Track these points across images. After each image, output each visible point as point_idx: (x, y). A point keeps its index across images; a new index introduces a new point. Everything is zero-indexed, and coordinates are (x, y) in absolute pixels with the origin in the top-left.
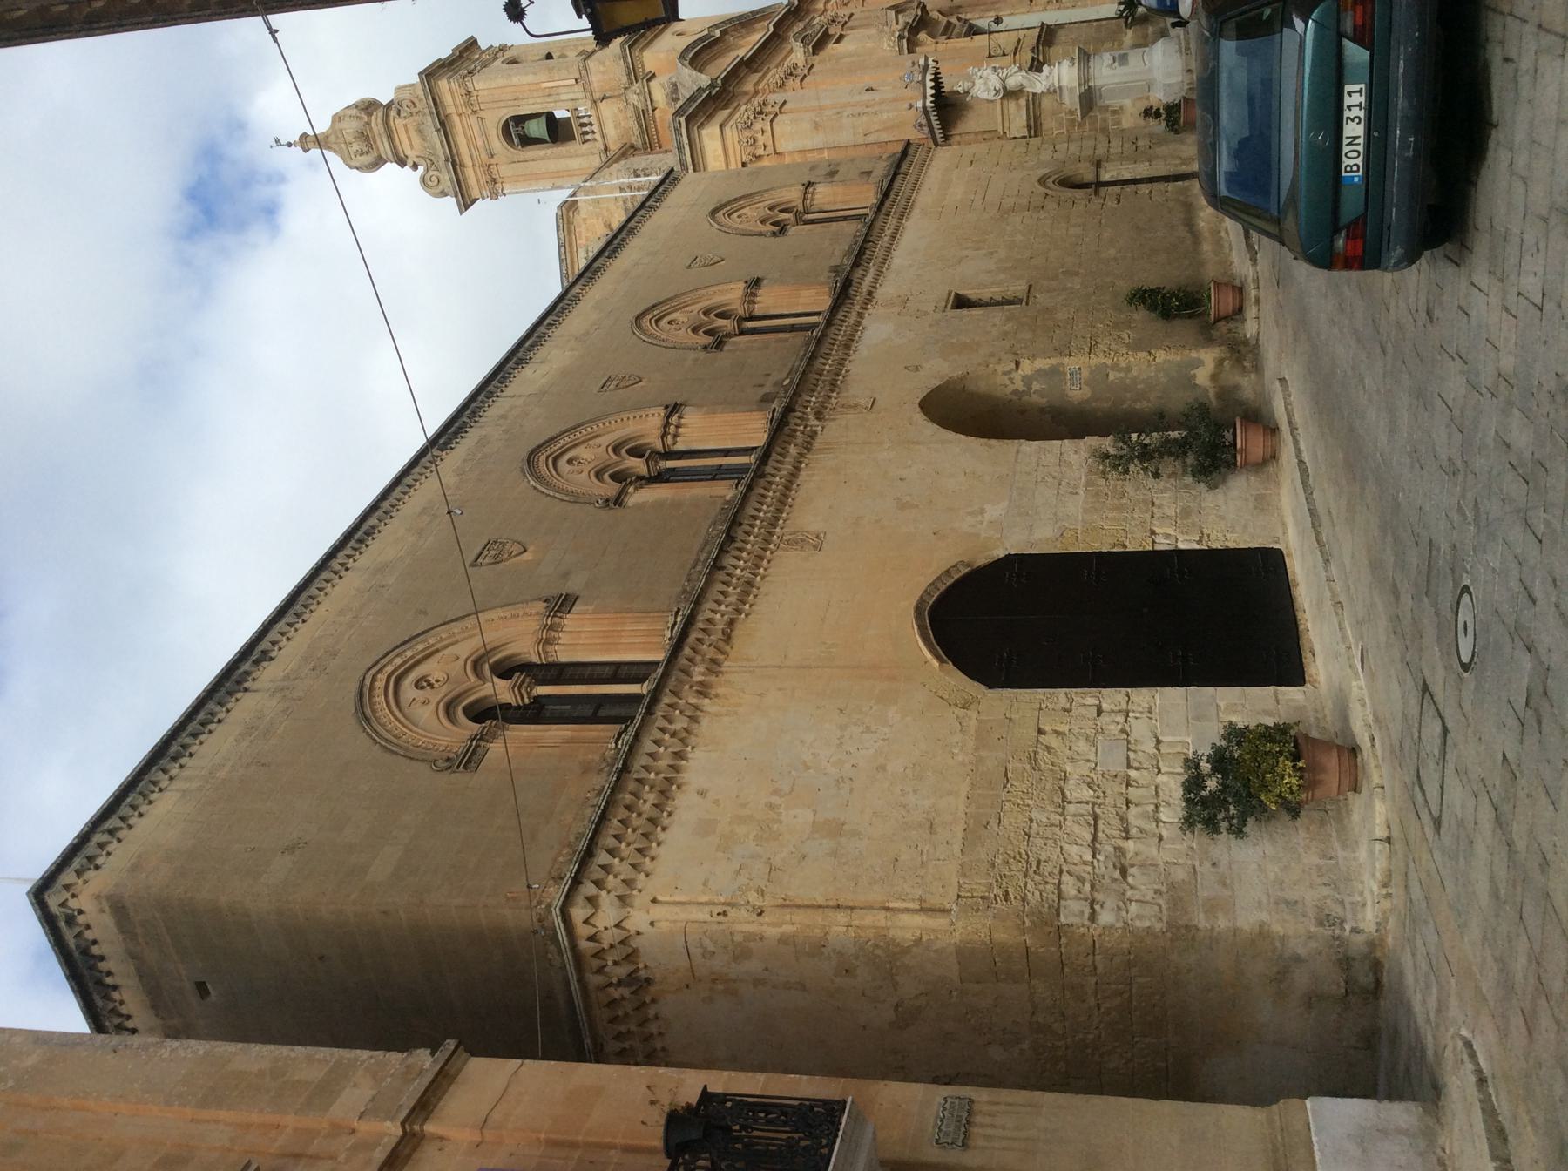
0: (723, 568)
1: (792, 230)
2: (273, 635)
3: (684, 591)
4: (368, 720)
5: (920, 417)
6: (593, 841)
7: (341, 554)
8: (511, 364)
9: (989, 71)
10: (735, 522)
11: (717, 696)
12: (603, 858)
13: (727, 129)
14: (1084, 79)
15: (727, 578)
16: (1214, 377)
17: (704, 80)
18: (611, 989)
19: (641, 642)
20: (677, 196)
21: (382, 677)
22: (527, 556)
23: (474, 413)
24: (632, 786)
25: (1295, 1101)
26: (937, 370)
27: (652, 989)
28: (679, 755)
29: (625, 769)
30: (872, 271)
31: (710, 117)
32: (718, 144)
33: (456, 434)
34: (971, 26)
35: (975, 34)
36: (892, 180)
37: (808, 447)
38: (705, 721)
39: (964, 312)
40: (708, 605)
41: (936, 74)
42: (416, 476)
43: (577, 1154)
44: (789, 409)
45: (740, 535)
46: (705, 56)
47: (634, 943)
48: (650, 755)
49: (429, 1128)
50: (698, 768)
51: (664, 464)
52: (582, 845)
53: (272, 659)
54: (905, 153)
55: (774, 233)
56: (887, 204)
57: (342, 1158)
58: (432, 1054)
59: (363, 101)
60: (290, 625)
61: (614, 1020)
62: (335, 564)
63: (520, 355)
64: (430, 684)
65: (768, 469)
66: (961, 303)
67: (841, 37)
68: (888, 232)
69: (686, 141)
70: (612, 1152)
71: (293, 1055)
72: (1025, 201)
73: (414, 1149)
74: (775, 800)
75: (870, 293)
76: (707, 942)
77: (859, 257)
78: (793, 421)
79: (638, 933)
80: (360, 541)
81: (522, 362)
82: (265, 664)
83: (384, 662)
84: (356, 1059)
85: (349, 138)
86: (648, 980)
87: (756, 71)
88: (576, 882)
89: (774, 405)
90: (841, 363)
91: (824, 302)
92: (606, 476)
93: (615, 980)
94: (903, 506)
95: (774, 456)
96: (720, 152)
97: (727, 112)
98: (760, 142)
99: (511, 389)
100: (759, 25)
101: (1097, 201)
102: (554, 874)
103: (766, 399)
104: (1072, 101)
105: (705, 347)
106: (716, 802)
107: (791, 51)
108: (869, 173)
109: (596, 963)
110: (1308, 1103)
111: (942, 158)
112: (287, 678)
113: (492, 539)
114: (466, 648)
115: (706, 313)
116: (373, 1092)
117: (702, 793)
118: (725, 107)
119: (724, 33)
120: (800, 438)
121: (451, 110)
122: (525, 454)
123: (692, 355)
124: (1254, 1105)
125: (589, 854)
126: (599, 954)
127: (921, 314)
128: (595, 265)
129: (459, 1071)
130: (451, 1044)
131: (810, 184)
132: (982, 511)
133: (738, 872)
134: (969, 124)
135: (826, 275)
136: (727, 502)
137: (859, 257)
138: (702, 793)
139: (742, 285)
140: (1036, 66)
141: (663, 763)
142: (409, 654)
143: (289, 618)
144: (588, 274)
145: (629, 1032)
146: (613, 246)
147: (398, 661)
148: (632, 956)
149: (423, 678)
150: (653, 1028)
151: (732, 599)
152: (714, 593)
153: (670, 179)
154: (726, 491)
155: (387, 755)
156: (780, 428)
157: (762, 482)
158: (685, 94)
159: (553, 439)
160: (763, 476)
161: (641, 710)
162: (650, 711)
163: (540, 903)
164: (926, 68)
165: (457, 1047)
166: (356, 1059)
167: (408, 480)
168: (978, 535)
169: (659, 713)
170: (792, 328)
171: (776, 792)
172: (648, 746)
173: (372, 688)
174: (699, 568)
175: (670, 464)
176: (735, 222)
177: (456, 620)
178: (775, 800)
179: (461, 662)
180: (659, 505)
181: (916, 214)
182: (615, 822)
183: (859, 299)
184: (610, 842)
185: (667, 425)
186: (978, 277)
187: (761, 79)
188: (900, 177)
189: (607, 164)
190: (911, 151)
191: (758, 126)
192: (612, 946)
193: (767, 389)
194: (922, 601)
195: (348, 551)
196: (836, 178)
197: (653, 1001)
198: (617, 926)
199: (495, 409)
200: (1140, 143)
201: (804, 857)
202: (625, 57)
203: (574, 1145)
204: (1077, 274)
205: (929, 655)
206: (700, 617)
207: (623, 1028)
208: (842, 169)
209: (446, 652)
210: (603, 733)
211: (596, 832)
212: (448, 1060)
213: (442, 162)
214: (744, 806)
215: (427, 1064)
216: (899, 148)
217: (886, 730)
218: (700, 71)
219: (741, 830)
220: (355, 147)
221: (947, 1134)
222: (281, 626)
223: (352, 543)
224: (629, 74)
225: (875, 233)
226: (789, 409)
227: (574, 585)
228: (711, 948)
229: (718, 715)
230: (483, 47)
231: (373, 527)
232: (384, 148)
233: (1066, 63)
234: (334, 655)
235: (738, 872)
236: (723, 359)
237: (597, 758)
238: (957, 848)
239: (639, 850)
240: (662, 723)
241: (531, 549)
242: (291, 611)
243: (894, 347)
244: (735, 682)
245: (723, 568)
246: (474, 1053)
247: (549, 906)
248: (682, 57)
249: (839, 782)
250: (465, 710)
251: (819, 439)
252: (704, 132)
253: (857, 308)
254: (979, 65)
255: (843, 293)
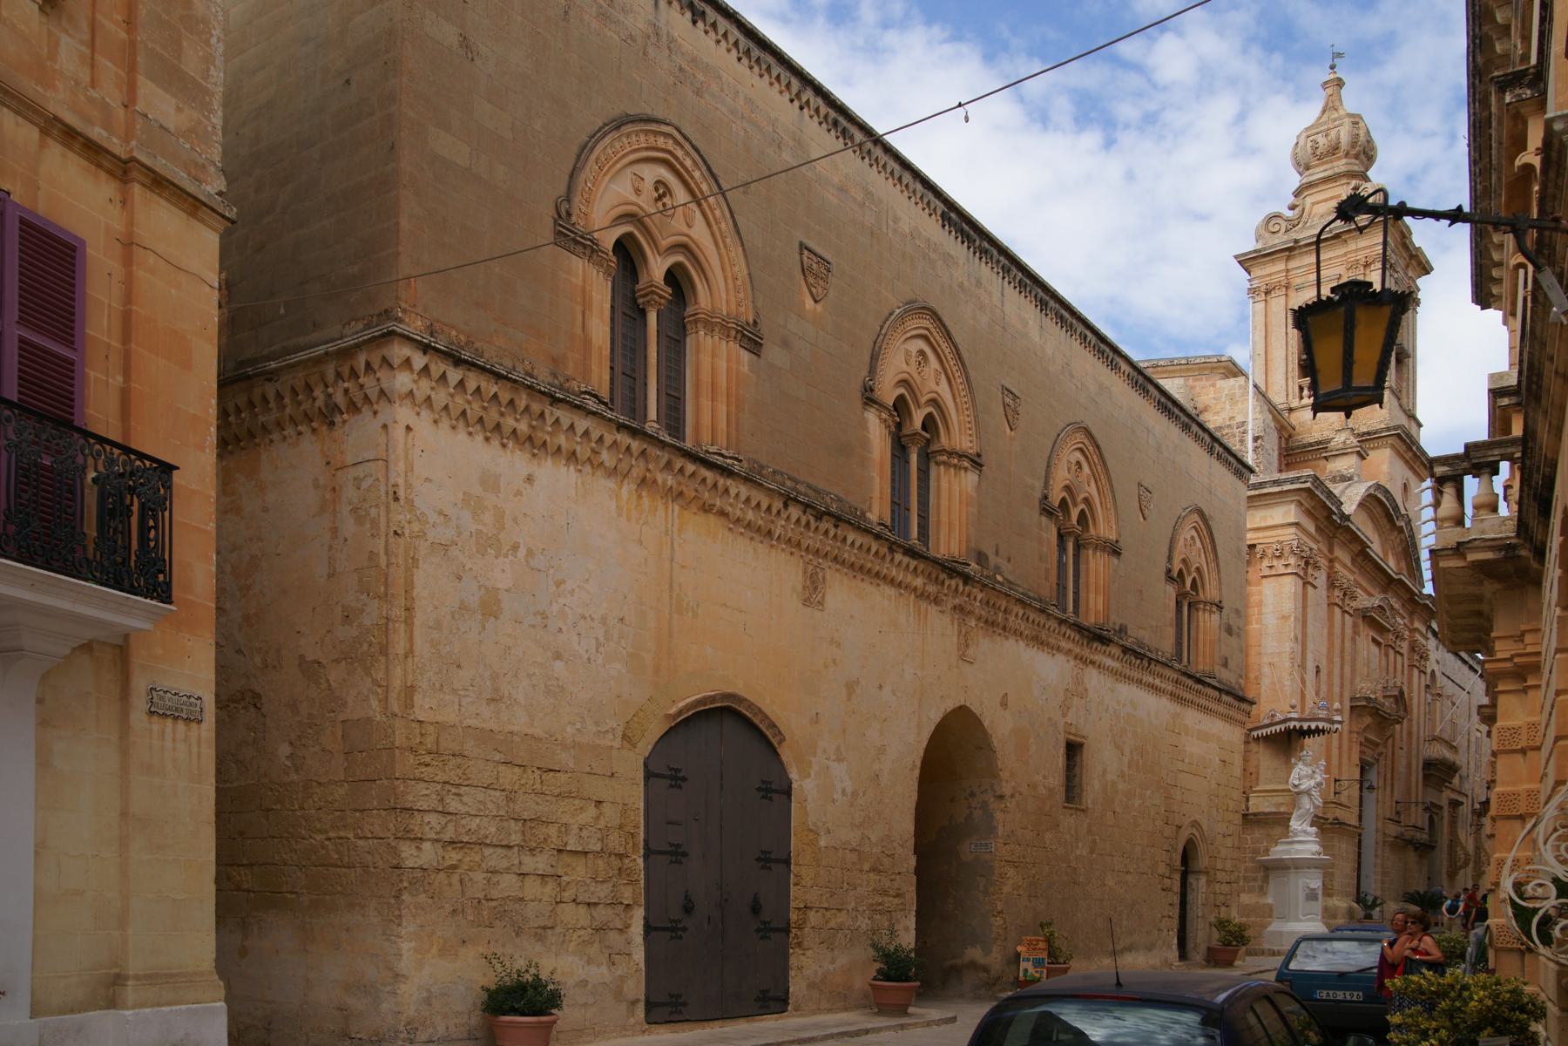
0: (786, 506)
1: (1171, 591)
2: (723, 24)
3: (762, 467)
4: (618, 128)
5: (950, 705)
6: (472, 365)
7: (820, 101)
8: (1041, 294)
9: (1319, 778)
10: (838, 520)
11: (640, 497)
12: (454, 375)
13: (1293, 530)
14: (1298, 865)
15: (774, 511)
16: (973, 965)
17: (1349, 508)
18: (322, 387)
19: (708, 421)
20: (1222, 475)
21: (670, 145)
22: (809, 303)
23: (986, 252)
24: (536, 407)
25: (222, 993)
26: (999, 725)
27: (325, 428)
28: (572, 457)
29: (555, 401)
30: (1116, 665)
31: (1309, 513)
32: (1278, 523)
33: (962, 231)
34: (1371, 765)
35: (1362, 769)
36: (1214, 687)
37: (921, 595)
38: (610, 484)
39: (1062, 751)
40: (744, 491)
41: (1323, 731)
42: (912, 186)
43: (116, 344)
44: (967, 579)
45: (825, 525)
46: (1378, 510)
47: (366, 412)
48: (572, 427)
49: (137, 189)
50: (555, 477)
51: (917, 443)
52: (465, 355)
53: (694, 22)
54: (1242, 699)
55: (1169, 571)
56: (1190, 682)
57: (94, 93)
58: (220, 194)
59: (1373, 149)
60: (736, 44)
61: (294, 392)
62: (808, 94)
63: (1052, 303)
64: (660, 198)
65: (898, 557)
66: (1073, 749)
67: (1378, 644)
68: (1157, 682)
69: (1286, 488)
70: (120, 379)
71: (214, 41)
72: (1175, 808)
73: (110, 172)
74: (522, 552)
75: (1093, 663)
76: (370, 481)
77: (1137, 654)
78: (953, 582)
79: (375, 413)
80: (835, 123)
81: (1043, 305)
82: (688, 15)
83: (687, 146)
84: (211, 112)
85: (1333, 133)
86: (332, 424)
87: (1353, 561)
88: (426, 348)
89: (974, 565)
90: (1019, 634)
91: (1090, 619)
92: (902, 391)
93: (330, 390)
94: (851, 686)
95: (913, 563)
96: (1270, 522)
97: (1312, 529)
98: (1275, 562)
99: (1011, 293)
100: (1403, 564)
101: (1162, 869)
102: (437, 326)
103: (981, 558)
104: (1279, 851)
105: (1046, 497)
106: (519, 493)
107: (1370, 595)
108: (1225, 665)
109: (346, 371)
110: (222, 1004)
111: (1233, 735)
112: (672, 40)
113: (834, 268)
114: (699, 233)
115: (1086, 500)
116: (172, 129)
117: (529, 479)
118: (1318, 528)
119: (1400, 530)
120: (931, 588)
121: (1352, 246)
122: (932, 304)
123: (1039, 484)
124: (217, 960)
125: (458, 362)
126: (354, 374)
127: (1065, 708)
128: (1151, 388)
129: (202, 221)
130: (232, 213)
131: (1220, 608)
132: (840, 760)
133: (441, 513)
134: (1265, 760)
135: (1116, 620)
136: (863, 514)
137: (1137, 654)
138: (529, 479)
139: (1113, 537)
140: (1319, 821)
141: (562, 440)
142: (697, 174)
143: (744, 42)
144: (1141, 380)
145: (284, 407)
146: (1169, 406)
147: (688, 163)
148: (354, 408)
149: (668, 191)
150: (289, 431)
151: (750, 515)
152: (757, 496)
153: (1242, 469)
154: (878, 511)
155: (575, 150)
156: (951, 569)
157: (884, 550)
158: (1336, 489)
159: (948, 336)
160: (891, 550)
161: (622, 419)
162: (621, 427)
163: (404, 311)
164: (1333, 722)
165: (228, 219)
166: (211, 112)
167: (907, 178)
168: (815, 754)
169: (619, 437)
170: (1061, 587)
171: (530, 553)
172: (582, 424)
173: (656, 133)
174: (789, 483)
175: (914, 458)
176: (1187, 533)
177: (735, 225)
178: (522, 552)
179: (685, 229)
180: (865, 443)
181: (1177, 708)
182: (494, 389)
183: (1086, 652)
184: (471, 385)
185: (961, 456)
186: (1103, 763)
187: (1345, 566)
188: (1217, 694)
189: (1272, 408)
190: (1244, 706)
191: (1292, 560)
192: (362, 386)
193: (993, 560)
194: (741, 700)
195: (824, 109)
196: (1224, 634)
197: (314, 430)
198: (382, 392)
199: (986, 273)
200: (1223, 909)
201: (460, 578)
202: (1388, 429)
203: (126, 338)
204: (1092, 852)
205: (681, 705)
206: (729, 482)
207: (287, 400)
208: (1233, 641)
209: (698, 215)
210: (600, 378)
211: (483, 369)
212: (213, 210)
213: (1294, 235)
214: (515, 520)
215: (208, 188)
216: (1250, 695)
217: (600, 661)
218: (1361, 505)
219: (488, 518)
220: (1321, 140)
221: (161, 698)
222: (735, 33)
223: (833, 114)
224: (1368, 433)
225: (1159, 669)
226: (967, 579)
227: (772, 352)
228: (364, 485)
229: (618, 497)
230: (1419, 282)
231: (852, 138)
232: (1318, 173)
233: (1316, 848)
234: (698, 93)
235: (441, 513)
236: (1033, 515)
237: (570, 372)
238: (473, 722)
239: (464, 413)
240: (608, 439)
241: (819, 308)
242: (751, 45)
243: (1026, 685)
244: (660, 516)
245: (786, 506)
246: (225, 239)
247: (400, 320)
248: (1379, 487)
249: (544, 616)
250: (630, 235)
251: (933, 609)
252: (1293, 506)
253: (1077, 650)
254: (1327, 770)
255: (1098, 637)
